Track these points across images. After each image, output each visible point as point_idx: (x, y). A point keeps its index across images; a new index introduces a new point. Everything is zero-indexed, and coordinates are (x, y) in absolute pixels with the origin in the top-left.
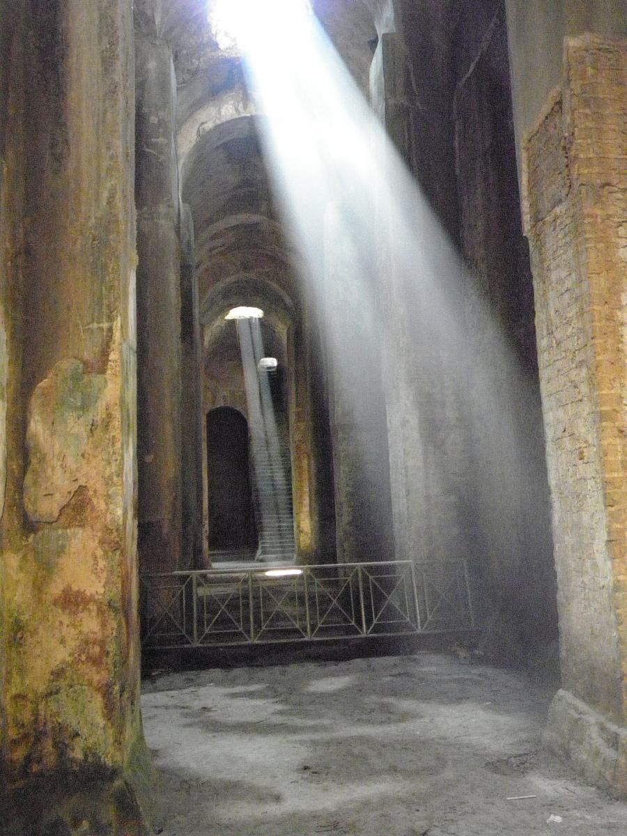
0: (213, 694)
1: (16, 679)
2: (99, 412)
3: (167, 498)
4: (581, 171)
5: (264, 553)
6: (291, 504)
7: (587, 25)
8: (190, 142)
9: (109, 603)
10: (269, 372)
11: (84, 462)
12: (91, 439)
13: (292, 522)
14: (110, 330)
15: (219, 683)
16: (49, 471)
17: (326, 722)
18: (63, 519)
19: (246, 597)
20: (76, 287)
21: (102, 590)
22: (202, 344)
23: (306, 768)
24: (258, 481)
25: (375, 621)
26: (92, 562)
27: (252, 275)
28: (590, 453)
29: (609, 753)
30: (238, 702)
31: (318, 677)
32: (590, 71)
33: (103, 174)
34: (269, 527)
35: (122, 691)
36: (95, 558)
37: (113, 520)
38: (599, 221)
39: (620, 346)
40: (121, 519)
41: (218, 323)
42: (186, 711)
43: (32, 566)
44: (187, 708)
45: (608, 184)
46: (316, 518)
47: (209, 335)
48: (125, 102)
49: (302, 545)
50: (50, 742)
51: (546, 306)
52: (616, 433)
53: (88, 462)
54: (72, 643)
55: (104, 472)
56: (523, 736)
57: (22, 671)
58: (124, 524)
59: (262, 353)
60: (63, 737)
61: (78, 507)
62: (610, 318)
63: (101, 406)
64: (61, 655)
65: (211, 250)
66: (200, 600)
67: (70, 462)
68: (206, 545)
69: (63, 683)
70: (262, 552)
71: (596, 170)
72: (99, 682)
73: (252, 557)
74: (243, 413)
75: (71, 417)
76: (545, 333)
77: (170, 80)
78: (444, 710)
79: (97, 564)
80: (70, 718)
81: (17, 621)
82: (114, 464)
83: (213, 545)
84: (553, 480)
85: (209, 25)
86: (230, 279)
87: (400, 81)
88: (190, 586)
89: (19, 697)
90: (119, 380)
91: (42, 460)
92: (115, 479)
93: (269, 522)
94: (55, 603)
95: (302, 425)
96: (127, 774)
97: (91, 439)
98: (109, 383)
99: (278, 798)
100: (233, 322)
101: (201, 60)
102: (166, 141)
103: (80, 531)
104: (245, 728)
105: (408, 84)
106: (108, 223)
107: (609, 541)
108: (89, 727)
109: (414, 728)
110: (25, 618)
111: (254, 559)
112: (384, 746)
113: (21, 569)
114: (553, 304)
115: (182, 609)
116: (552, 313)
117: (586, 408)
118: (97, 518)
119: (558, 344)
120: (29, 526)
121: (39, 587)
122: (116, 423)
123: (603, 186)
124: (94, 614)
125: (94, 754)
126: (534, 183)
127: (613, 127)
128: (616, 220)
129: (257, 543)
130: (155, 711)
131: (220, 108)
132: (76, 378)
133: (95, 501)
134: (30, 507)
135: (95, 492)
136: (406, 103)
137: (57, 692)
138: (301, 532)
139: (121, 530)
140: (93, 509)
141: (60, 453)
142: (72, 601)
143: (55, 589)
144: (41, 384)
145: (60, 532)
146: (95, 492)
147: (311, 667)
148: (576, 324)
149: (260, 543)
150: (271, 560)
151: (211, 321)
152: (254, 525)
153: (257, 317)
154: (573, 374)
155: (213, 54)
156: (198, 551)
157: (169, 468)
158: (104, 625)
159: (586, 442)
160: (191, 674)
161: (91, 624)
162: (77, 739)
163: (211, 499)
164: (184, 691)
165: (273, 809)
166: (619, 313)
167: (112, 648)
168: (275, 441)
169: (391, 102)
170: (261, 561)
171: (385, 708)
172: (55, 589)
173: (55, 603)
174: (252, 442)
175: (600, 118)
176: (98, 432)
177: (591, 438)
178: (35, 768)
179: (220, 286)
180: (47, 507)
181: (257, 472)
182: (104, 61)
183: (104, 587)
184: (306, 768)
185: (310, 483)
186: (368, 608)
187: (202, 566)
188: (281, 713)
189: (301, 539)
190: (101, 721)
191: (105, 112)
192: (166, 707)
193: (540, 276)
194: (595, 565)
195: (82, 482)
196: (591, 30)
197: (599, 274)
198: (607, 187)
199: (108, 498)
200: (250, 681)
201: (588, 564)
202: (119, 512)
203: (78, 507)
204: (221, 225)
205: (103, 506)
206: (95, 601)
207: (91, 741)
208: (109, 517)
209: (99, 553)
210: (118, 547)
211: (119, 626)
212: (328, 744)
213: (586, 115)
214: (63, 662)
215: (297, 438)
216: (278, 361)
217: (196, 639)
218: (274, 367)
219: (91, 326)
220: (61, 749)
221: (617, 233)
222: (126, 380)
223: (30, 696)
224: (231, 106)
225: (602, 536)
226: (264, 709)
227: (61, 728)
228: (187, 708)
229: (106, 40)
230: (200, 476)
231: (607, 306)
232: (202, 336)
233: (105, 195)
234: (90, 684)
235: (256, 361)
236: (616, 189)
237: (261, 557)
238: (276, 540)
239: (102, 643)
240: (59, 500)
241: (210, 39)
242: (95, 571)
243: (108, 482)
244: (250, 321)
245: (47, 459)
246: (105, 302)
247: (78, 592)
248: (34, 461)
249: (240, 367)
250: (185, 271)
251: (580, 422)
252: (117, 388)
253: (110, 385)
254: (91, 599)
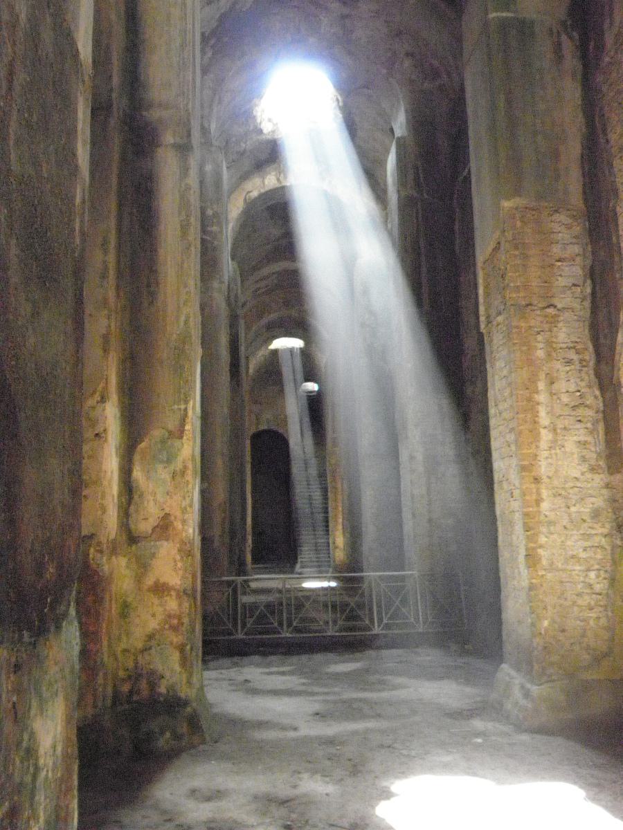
0: (253, 671)
1: (124, 638)
2: (178, 465)
3: (218, 517)
4: (511, 296)
5: (302, 567)
6: (327, 522)
7: (517, 192)
8: (238, 208)
9: (184, 591)
10: (308, 396)
11: (168, 497)
12: (173, 483)
13: (328, 538)
14: (186, 409)
15: (258, 665)
16: (146, 503)
17: (336, 689)
18: (154, 536)
19: (281, 604)
20: (164, 381)
21: (179, 583)
22: (247, 372)
23: (317, 714)
25: (385, 621)
26: (173, 564)
28: (517, 493)
29: (523, 702)
30: (273, 677)
31: (336, 663)
32: (519, 224)
33: (181, 306)
34: (308, 543)
35: (192, 649)
36: (175, 561)
37: (186, 536)
38: (523, 330)
39: (537, 419)
40: (192, 536)
42: (231, 682)
43: (134, 566)
44: (233, 680)
45: (531, 305)
47: (253, 364)
48: (194, 234)
49: (337, 559)
50: (145, 681)
51: (493, 385)
52: (532, 480)
53: (171, 498)
54: (160, 617)
55: (181, 505)
56: (478, 699)
57: (128, 634)
58: (193, 539)
59: (302, 378)
60: (154, 678)
61: (164, 527)
62: (529, 400)
63: (180, 459)
64: (153, 624)
66: (244, 606)
67: (160, 498)
68: (249, 558)
69: (153, 643)
71: (522, 294)
72: (177, 642)
75: (160, 467)
76: (493, 404)
78: (427, 684)
79: (176, 565)
80: (159, 667)
81: (125, 602)
82: (187, 498)
83: (256, 560)
84: (498, 513)
85: (255, 117)
86: (273, 316)
87: (411, 177)
88: (235, 591)
89: (125, 651)
90: (191, 444)
91: (141, 496)
92: (188, 509)
94: (149, 590)
96: (194, 704)
97: (173, 483)
98: (185, 445)
99: (296, 729)
100: (275, 352)
101: (248, 143)
102: (219, 230)
103: (165, 543)
104: (276, 693)
105: (417, 179)
106: (185, 338)
107: (526, 555)
108: (171, 670)
109: (401, 694)
110: (130, 600)
112: (376, 703)
113: (127, 567)
114: (498, 385)
115: (228, 606)
116: (497, 390)
117: (514, 462)
118: (176, 534)
119: (500, 413)
120: (133, 539)
121: (139, 579)
122: (189, 472)
123: (528, 305)
124: (174, 598)
125: (174, 691)
126: (487, 294)
127: (534, 263)
128: (536, 329)
129: (296, 558)
130: (210, 682)
131: (264, 179)
132: (163, 442)
133: (175, 523)
134: (133, 527)
135: (175, 518)
136: (415, 195)
137: (150, 648)
138: (336, 547)
139: (191, 543)
140: (174, 528)
141: (153, 490)
142: (160, 589)
143: (149, 581)
144: (141, 445)
145: (152, 543)
146: (175, 518)
147: (330, 656)
148: (509, 402)
149: (299, 557)
151: (258, 349)
152: (295, 541)
153: (298, 347)
154: (508, 436)
155: (259, 137)
156: (242, 563)
157: (221, 493)
158: (180, 605)
159: (514, 485)
160: (236, 659)
161: (172, 604)
162: (163, 680)
163: (254, 518)
164: (231, 670)
165: (292, 734)
166: (536, 396)
167: (186, 620)
168: (313, 462)
169: (403, 194)
171: (381, 682)
172: (149, 581)
173: (149, 590)
174: (293, 462)
175: (526, 257)
176: (178, 478)
177: (517, 484)
178: (135, 698)
179: (265, 321)
180: (144, 526)
181: (297, 491)
182: (182, 227)
183: (180, 580)
184: (317, 714)
186: (379, 613)
187: (244, 573)
188: (304, 684)
190: (177, 668)
191: (182, 263)
192: (217, 680)
194: (520, 573)
195: (167, 510)
196: (520, 196)
197: (522, 368)
198: (529, 307)
199: (184, 522)
200: (283, 664)
201: (516, 571)
202: (191, 531)
203: (164, 527)
204: (265, 271)
205: (180, 527)
206: (175, 590)
207: (171, 681)
208: (184, 535)
209: (178, 557)
210: (189, 554)
211: (190, 606)
212: (335, 702)
213: (515, 256)
214: (154, 629)
216: (320, 386)
217: (239, 631)
218: (314, 392)
219: (173, 407)
220: (152, 686)
221: (536, 339)
222: (195, 442)
223: (133, 650)
224: (274, 177)
225: (523, 552)
226: (293, 681)
227: (152, 673)
228: (233, 680)
229: (183, 213)
230: (244, 500)
231: (527, 391)
232: (248, 368)
233: (183, 318)
234: (172, 644)
235: (297, 386)
236: (536, 308)
238: (313, 556)
239: (179, 618)
240: (152, 522)
241: (256, 127)
242: (175, 570)
243: (184, 511)
244: (291, 351)
245: (144, 495)
246: (183, 391)
247: (164, 583)
248: (136, 497)
249: (281, 391)
250: (233, 320)
251: (511, 471)
252: (189, 449)
253: (185, 446)
254: (173, 588)
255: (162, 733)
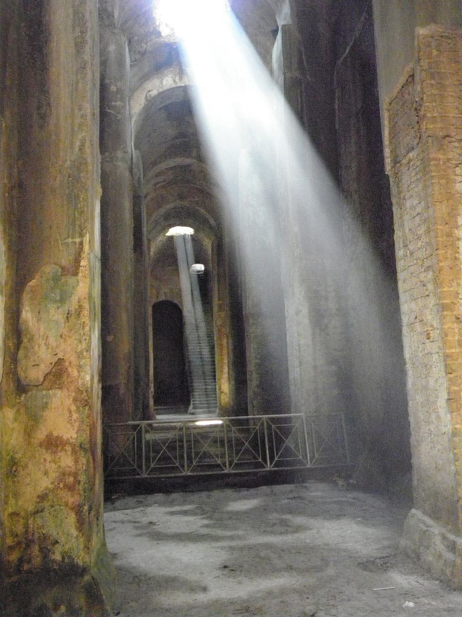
0: (157, 512)
1: (12, 501)
2: (73, 304)
3: (123, 367)
4: (428, 126)
5: (195, 408)
6: (214, 372)
7: (433, 18)
8: (140, 105)
9: (81, 445)
10: (199, 275)
11: (62, 341)
12: (67, 324)
13: (216, 385)
14: (81, 243)
15: (162, 504)
16: (36, 348)
17: (240, 533)
18: (46, 383)
19: (181, 441)
20: (56, 212)
21: (75, 436)
22: (149, 254)
23: (225, 567)
24: (190, 355)
25: (276, 459)
26: (68, 415)
27: (186, 203)
28: (435, 334)
29: (449, 556)
30: (175, 518)
31: (235, 500)
32: (435, 53)
33: (76, 129)
34: (198, 389)
35: (90, 510)
36: (70, 412)
37: (83, 384)
38: (442, 163)
39: (457, 255)
40: (89, 383)
41: (161, 238)
42: (137, 524)
43: (23, 418)
44: (138, 522)
45: (448, 136)
46: (233, 382)
47: (154, 248)
48: (92, 75)
49: (223, 402)
50: (37, 547)
51: (402, 226)
52: (454, 319)
53: (65, 341)
54: (53, 475)
55: (77, 348)
56: (386, 543)
57: (16, 495)
58: (92, 387)
59: (193, 261)
60: (47, 544)
61: (57, 374)
62: (449, 235)
63: (74, 300)
64: (45, 483)
65: (155, 185)
66: (148, 443)
67: (52, 341)
68: (151, 402)
69: (46, 504)
70: (193, 407)
71: (439, 125)
72: (73, 503)
73: (186, 411)
74: (179, 305)
75: (52, 308)
76: (401, 246)
77: (125, 59)
78: (327, 524)
79: (71, 417)
80: (52, 530)
81: (12, 458)
82: (84, 343)
83: (157, 402)
84: (407, 354)
85: (154, 18)
86: (169, 206)
87: (295, 60)
88: (140, 433)
89: (14, 514)
90: (88, 280)
91: (31, 339)
92: (85, 353)
93: (198, 385)
94: (41, 445)
95: (223, 314)
96: (94, 571)
97: (67, 324)
98: (80, 283)
99: (205, 589)
100: (172, 237)
101: (148, 44)
102: (123, 104)
103: (59, 392)
104: (180, 538)
105: (300, 62)
106: (80, 165)
107: (449, 399)
108: (66, 536)
109: (305, 537)
110: (18, 456)
111: (187, 412)
112: (283, 550)
113: (15, 420)
114: (408, 225)
115: (134, 449)
116: (407, 231)
117: (432, 301)
118: (71, 382)
119: (411, 254)
120: (21, 388)
121: (28, 433)
122: (86, 312)
123: (445, 137)
124: (69, 453)
125: (69, 557)
126: (393, 135)
127: (452, 94)
128: (454, 162)
129: (189, 401)
130: (114, 525)
131: (162, 80)
132: (56, 279)
133: (70, 370)
134: (22, 374)
135: (70, 363)
136: (299, 76)
137: (42, 511)
138: (222, 392)
139: (89, 391)
140: (68, 375)
141: (44, 334)
142: (53, 444)
143: (41, 435)
144: (30, 284)
145: (44, 392)
146: (70, 363)
147: (229, 492)
148: (425, 239)
149: (191, 400)
150: (200, 413)
151: (155, 237)
152: (187, 387)
153: (190, 234)
154: (422, 276)
155: (157, 40)
156: (146, 407)
157: (125, 346)
158: (76, 461)
159: (432, 326)
160: (141, 498)
161: (67, 461)
162: (57, 546)
163: (155, 368)
164: (136, 510)
165: (201, 597)
166: (456, 231)
167: (82, 478)
168: (202, 325)
169: (288, 75)
170: (193, 414)
171: (284, 523)
172: (41, 435)
173: (41, 445)
174: (186, 326)
175: (442, 87)
176: (73, 319)
177: (435, 323)
178: (26, 567)
179: (162, 211)
180: (35, 374)
181: (190, 348)
182: (76, 45)
183: (77, 433)
184: (225, 567)
185: (229, 357)
186: (271, 448)
187: (149, 418)
188: (207, 526)
189: (222, 398)
190: (74, 532)
191: (77, 83)
192: (123, 522)
193: (398, 204)
194: (438, 417)
195: (60, 356)
196: (436, 22)
197: (441, 202)
198: (447, 138)
199: (80, 368)
200: (184, 503)
201: (433, 416)
202: (88, 378)
203: (57, 374)
204: (162, 166)
205: (76, 373)
206: (70, 444)
207: (67, 547)
208: (80, 381)
209: (73, 408)
210: (87, 403)
211: (88, 462)
212: (241, 549)
213: (432, 85)
214: (47, 488)
215: (219, 323)
216: (205, 266)
217: (144, 471)
218: (202, 271)
219: (67, 241)
220: (45, 553)
221: (455, 172)
222: (93, 281)
223: (22, 514)
224: (170, 78)
225: (444, 395)
226: (194, 523)
227: (45, 537)
228: (138, 522)
229: (78, 29)
230: (147, 352)
231: (447, 226)
232: (149, 248)
233: (78, 144)
234: (66, 505)
235: (189, 266)
236: (454, 140)
237: (192, 411)
238: (203, 399)
239: (75, 475)
240: (43, 369)
241: (155, 29)
242: (70, 421)
243: (80, 356)
244: (184, 237)
245: (35, 339)
246: (78, 223)
247: (58, 437)
248: (25, 340)
249: (177, 271)
250: (137, 200)
251: (427, 312)
252: (86, 286)
253: (81, 284)
254: (67, 442)
255: (56, 607)
